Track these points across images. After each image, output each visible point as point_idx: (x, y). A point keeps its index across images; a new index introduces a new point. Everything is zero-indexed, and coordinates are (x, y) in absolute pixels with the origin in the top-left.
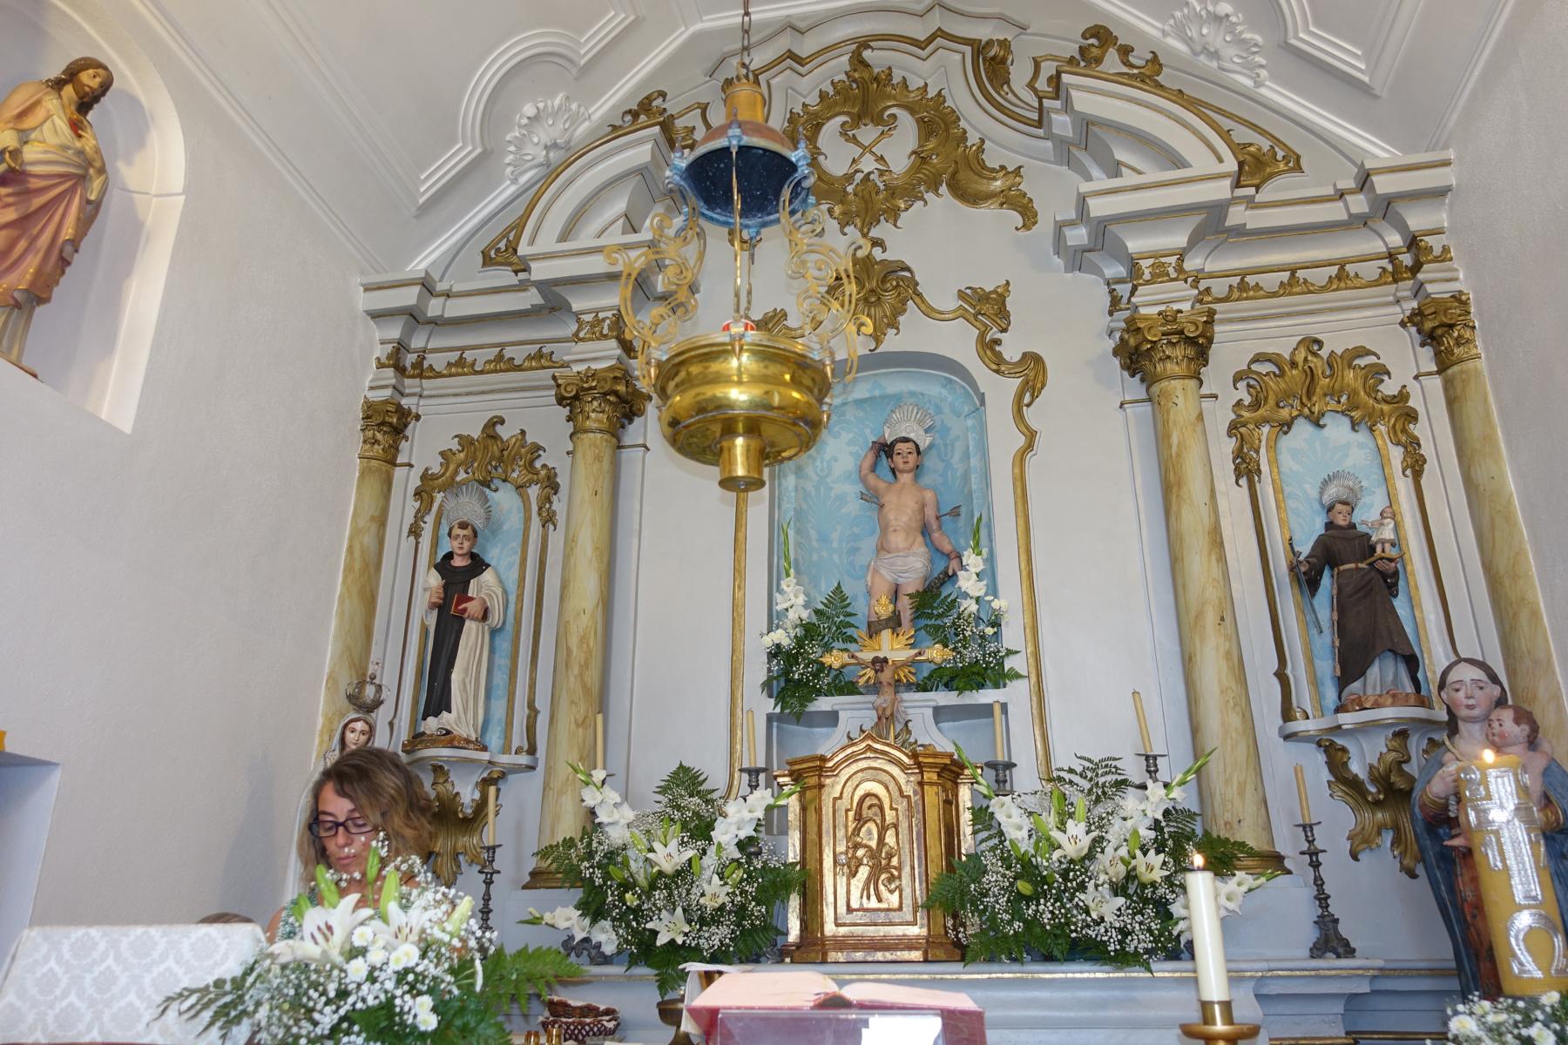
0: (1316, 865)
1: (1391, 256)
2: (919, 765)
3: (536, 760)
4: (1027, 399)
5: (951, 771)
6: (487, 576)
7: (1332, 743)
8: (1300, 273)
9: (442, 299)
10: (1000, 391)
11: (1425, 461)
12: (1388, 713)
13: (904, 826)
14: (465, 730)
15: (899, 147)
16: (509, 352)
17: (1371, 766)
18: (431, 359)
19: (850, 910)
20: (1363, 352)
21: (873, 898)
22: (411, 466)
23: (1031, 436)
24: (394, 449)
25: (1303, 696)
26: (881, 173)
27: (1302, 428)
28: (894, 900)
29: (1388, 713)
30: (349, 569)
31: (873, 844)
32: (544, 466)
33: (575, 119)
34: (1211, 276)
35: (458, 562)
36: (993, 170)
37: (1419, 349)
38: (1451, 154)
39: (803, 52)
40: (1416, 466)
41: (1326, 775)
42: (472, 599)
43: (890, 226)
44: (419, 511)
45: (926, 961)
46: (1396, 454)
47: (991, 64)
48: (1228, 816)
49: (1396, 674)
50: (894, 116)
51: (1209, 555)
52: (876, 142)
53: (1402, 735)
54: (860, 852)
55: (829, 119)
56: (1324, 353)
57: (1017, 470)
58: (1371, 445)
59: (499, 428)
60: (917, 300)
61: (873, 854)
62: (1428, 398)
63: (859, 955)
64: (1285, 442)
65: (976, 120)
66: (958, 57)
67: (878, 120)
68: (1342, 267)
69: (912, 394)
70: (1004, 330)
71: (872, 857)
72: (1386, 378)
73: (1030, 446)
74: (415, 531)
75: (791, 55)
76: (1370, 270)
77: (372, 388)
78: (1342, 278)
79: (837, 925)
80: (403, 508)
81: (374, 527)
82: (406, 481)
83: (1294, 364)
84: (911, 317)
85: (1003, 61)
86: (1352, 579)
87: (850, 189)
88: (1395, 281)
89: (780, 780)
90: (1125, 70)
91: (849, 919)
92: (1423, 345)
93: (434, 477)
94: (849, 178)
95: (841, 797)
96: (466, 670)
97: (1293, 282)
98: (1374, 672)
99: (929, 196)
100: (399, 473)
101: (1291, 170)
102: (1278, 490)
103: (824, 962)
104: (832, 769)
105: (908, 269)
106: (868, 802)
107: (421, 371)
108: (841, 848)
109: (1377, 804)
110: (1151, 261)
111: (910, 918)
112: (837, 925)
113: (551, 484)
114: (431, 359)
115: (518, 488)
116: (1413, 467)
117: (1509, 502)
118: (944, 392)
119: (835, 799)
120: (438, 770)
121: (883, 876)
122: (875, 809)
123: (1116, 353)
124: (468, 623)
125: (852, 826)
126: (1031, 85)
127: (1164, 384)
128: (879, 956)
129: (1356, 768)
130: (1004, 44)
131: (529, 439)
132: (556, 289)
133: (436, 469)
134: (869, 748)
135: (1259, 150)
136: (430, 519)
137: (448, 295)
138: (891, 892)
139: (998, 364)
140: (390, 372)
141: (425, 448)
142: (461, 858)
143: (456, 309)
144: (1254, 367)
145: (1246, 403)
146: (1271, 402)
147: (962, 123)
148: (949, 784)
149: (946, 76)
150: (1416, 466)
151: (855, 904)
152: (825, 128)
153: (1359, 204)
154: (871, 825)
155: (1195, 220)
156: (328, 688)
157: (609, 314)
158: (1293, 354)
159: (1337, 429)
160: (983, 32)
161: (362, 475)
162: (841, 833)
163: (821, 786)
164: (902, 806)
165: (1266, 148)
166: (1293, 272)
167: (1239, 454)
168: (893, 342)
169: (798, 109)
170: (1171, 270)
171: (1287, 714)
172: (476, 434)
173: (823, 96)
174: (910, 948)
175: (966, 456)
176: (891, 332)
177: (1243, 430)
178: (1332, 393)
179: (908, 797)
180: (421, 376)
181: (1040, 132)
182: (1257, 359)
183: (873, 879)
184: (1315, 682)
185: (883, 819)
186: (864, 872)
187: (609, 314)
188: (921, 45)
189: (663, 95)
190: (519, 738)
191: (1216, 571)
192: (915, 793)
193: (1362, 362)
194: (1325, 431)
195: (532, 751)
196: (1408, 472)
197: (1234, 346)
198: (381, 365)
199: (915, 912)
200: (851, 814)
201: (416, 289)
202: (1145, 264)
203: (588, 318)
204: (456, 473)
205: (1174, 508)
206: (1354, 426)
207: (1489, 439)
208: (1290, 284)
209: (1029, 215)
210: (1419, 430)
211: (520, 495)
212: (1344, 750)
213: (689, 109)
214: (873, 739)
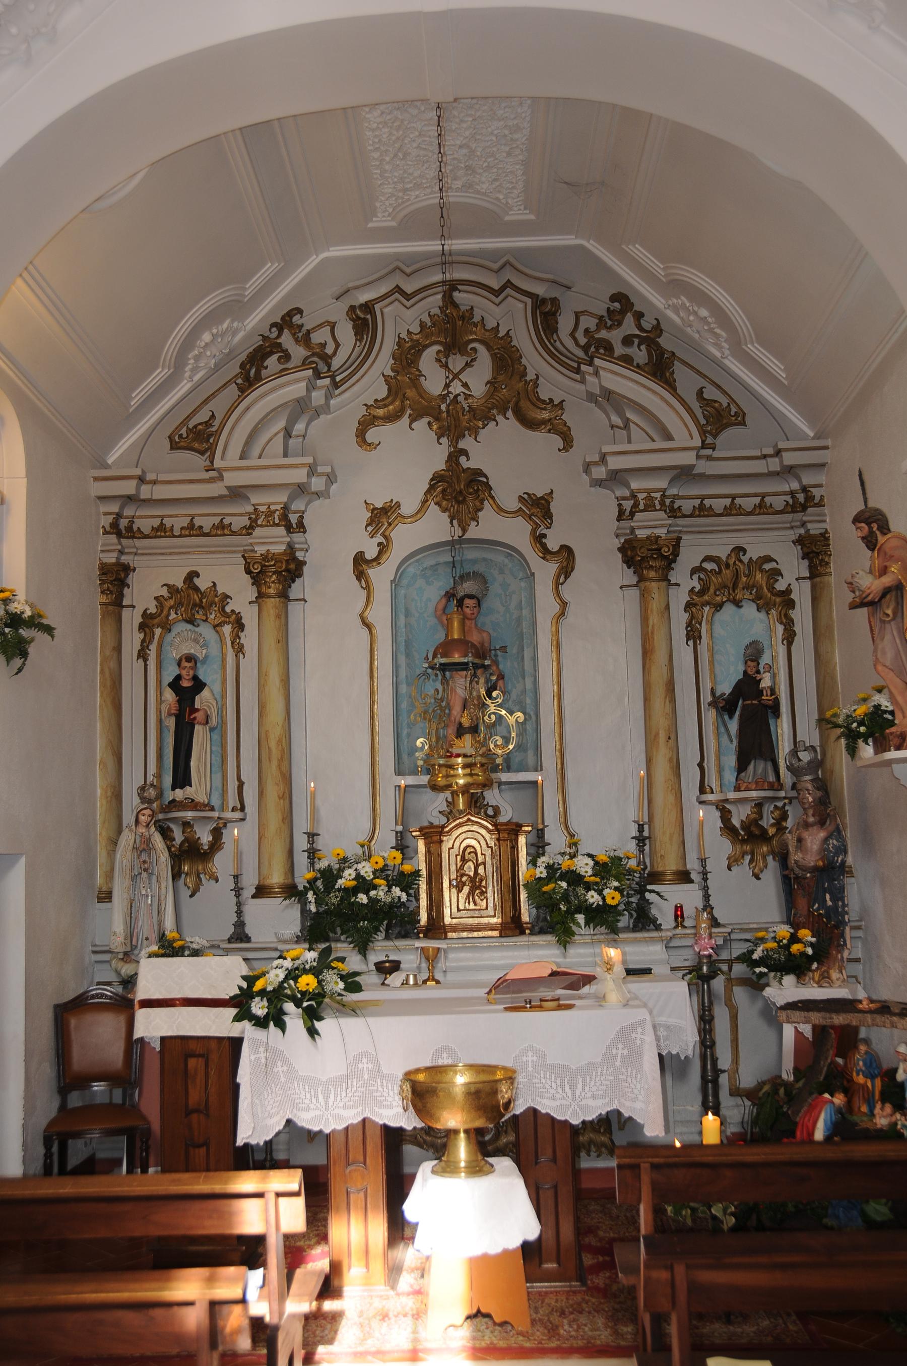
0: (705, 880)
1: (792, 493)
2: (498, 830)
3: (246, 814)
4: (562, 579)
5: (514, 830)
6: (205, 693)
7: (724, 807)
8: (738, 501)
9: (150, 486)
10: (545, 572)
11: (795, 634)
12: (754, 794)
13: (489, 865)
14: (201, 798)
15: (478, 379)
16: (198, 522)
17: (742, 821)
18: (138, 524)
19: (459, 910)
20: (768, 559)
21: (472, 903)
22: (134, 607)
23: (564, 604)
24: (121, 596)
25: (713, 780)
26: (467, 397)
27: (729, 608)
28: (484, 904)
29: (754, 794)
30: (103, 684)
31: (472, 874)
32: (233, 611)
33: (235, 332)
34: (683, 498)
35: (186, 684)
36: (544, 402)
37: (801, 560)
38: (829, 442)
39: (409, 290)
40: (790, 637)
41: (719, 824)
42: (198, 710)
43: (472, 439)
44: (143, 641)
45: (501, 936)
46: (780, 629)
47: (545, 314)
48: (662, 852)
49: (765, 769)
50: (474, 349)
51: (666, 698)
52: (462, 370)
53: (759, 805)
54: (464, 879)
55: (426, 347)
56: (745, 559)
57: (554, 629)
58: (767, 622)
59: (196, 580)
60: (491, 501)
61: (472, 880)
62: (802, 594)
63: (465, 934)
64: (718, 616)
65: (534, 360)
66: (521, 305)
67: (462, 351)
68: (762, 500)
69: (485, 560)
70: (548, 528)
71: (471, 881)
72: (780, 578)
73: (562, 613)
74: (143, 655)
75: (398, 289)
76: (778, 502)
77: (102, 551)
78: (762, 508)
79: (452, 918)
80: (132, 639)
81: (115, 655)
82: (131, 619)
83: (727, 566)
84: (487, 513)
85: (554, 314)
86: (749, 709)
87: (443, 407)
88: (793, 512)
89: (414, 834)
90: (638, 332)
91: (459, 915)
92: (803, 559)
93: (152, 616)
94: (443, 398)
95: (453, 848)
96: (199, 759)
97: (732, 510)
98: (751, 767)
99: (500, 418)
100: (126, 613)
101: (739, 424)
102: (712, 651)
103: (446, 938)
104: (448, 832)
105: (486, 477)
106: (469, 850)
107: (131, 533)
108: (453, 876)
109: (743, 842)
110: (645, 495)
111: (492, 914)
112: (452, 918)
113: (239, 625)
114: (138, 524)
115: (215, 627)
116: (787, 639)
117: (834, 669)
118: (506, 561)
119: (449, 849)
120: (186, 825)
121: (477, 892)
122: (472, 855)
123: (620, 550)
124: (196, 726)
125: (459, 864)
126: (572, 335)
127: (648, 583)
128: (475, 934)
129: (736, 822)
130: (555, 301)
131: (220, 590)
132: (241, 490)
133: (153, 610)
134: (469, 820)
135: (721, 405)
136: (153, 647)
137: (155, 482)
138: (482, 900)
139: (546, 553)
140: (113, 538)
141: (143, 593)
142: (202, 876)
143: (160, 492)
144: (705, 565)
145: (697, 590)
146: (712, 590)
147: (524, 361)
148: (513, 837)
149: (513, 319)
150: (790, 637)
151: (461, 907)
152: (425, 354)
153: (774, 464)
154: (470, 864)
155: (675, 472)
156: (101, 770)
157: (278, 507)
158: (727, 558)
159: (749, 610)
160: (540, 290)
161: (103, 617)
162: (453, 868)
163: (441, 841)
164: (488, 852)
165: (725, 405)
166: (734, 499)
167: (689, 624)
168: (473, 532)
169: (404, 335)
170: (657, 502)
171: (702, 791)
172: (180, 584)
173: (422, 325)
174: (492, 930)
175: (520, 607)
176: (474, 523)
177: (694, 609)
178: (748, 587)
179: (491, 847)
180: (133, 537)
181: (578, 377)
182: (707, 559)
183: (471, 893)
184: (720, 770)
185: (477, 860)
186: (466, 889)
187: (278, 507)
188: (497, 293)
189: (299, 311)
190: (232, 800)
191: (668, 708)
192: (495, 845)
193: (767, 567)
194: (742, 610)
195: (243, 809)
196: (785, 642)
197: (690, 555)
198: (106, 533)
199: (495, 910)
200: (459, 858)
201: (134, 483)
202: (641, 496)
203: (263, 509)
204: (169, 614)
205: (647, 666)
206: (759, 609)
207: (830, 628)
208: (731, 509)
209: (568, 442)
210: (795, 614)
211: (217, 632)
212: (730, 812)
213: (321, 326)
214: (472, 815)
